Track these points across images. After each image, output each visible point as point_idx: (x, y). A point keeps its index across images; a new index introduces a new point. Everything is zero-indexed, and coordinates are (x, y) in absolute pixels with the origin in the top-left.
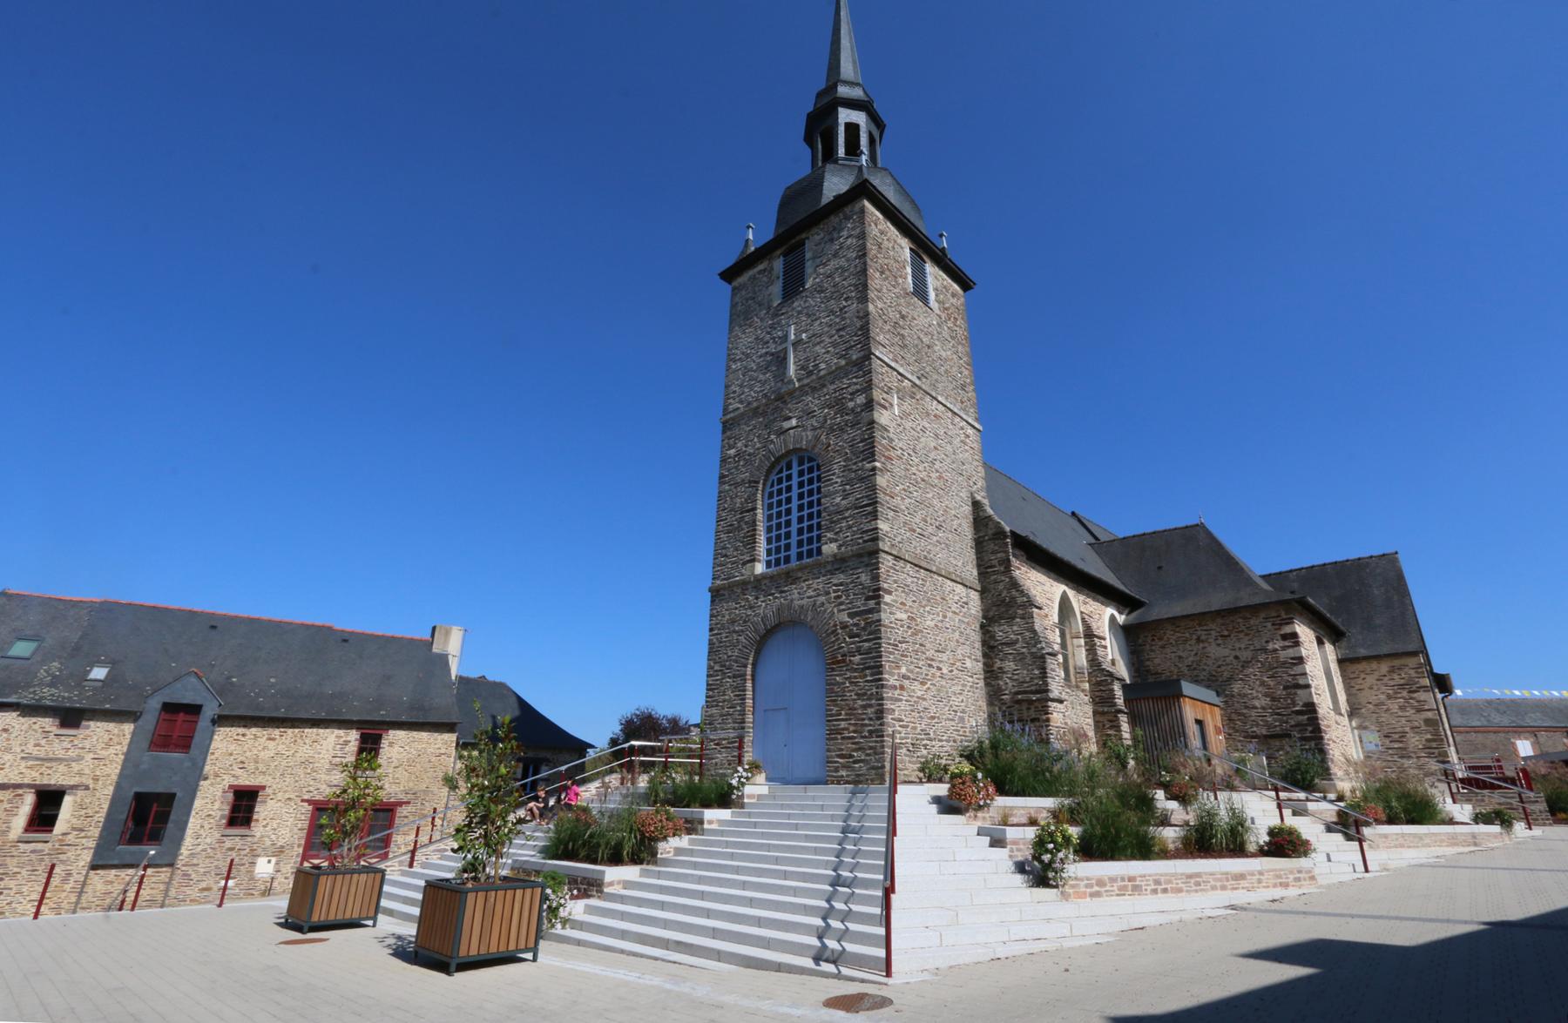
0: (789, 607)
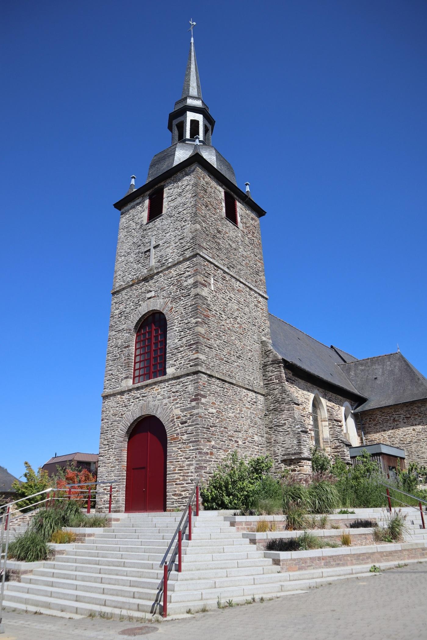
0: (148, 406)
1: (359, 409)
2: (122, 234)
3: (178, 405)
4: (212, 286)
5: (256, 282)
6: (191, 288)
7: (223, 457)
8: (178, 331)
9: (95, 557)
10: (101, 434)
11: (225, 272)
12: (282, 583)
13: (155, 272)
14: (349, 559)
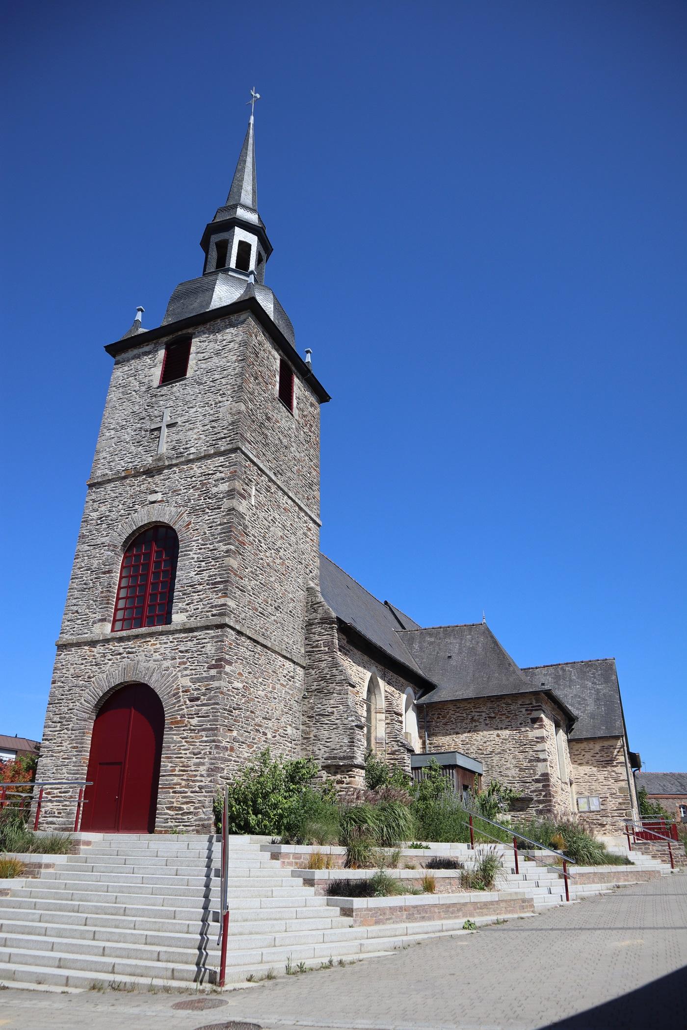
0: (135, 668)
1: (424, 699)
2: (114, 395)
3: (188, 672)
4: (253, 498)
5: (308, 499)
6: (224, 497)
7: (246, 755)
8: (196, 559)
9: (67, 900)
10: (50, 704)
11: (271, 480)
12: (363, 941)
13: (167, 463)
14: (437, 910)
